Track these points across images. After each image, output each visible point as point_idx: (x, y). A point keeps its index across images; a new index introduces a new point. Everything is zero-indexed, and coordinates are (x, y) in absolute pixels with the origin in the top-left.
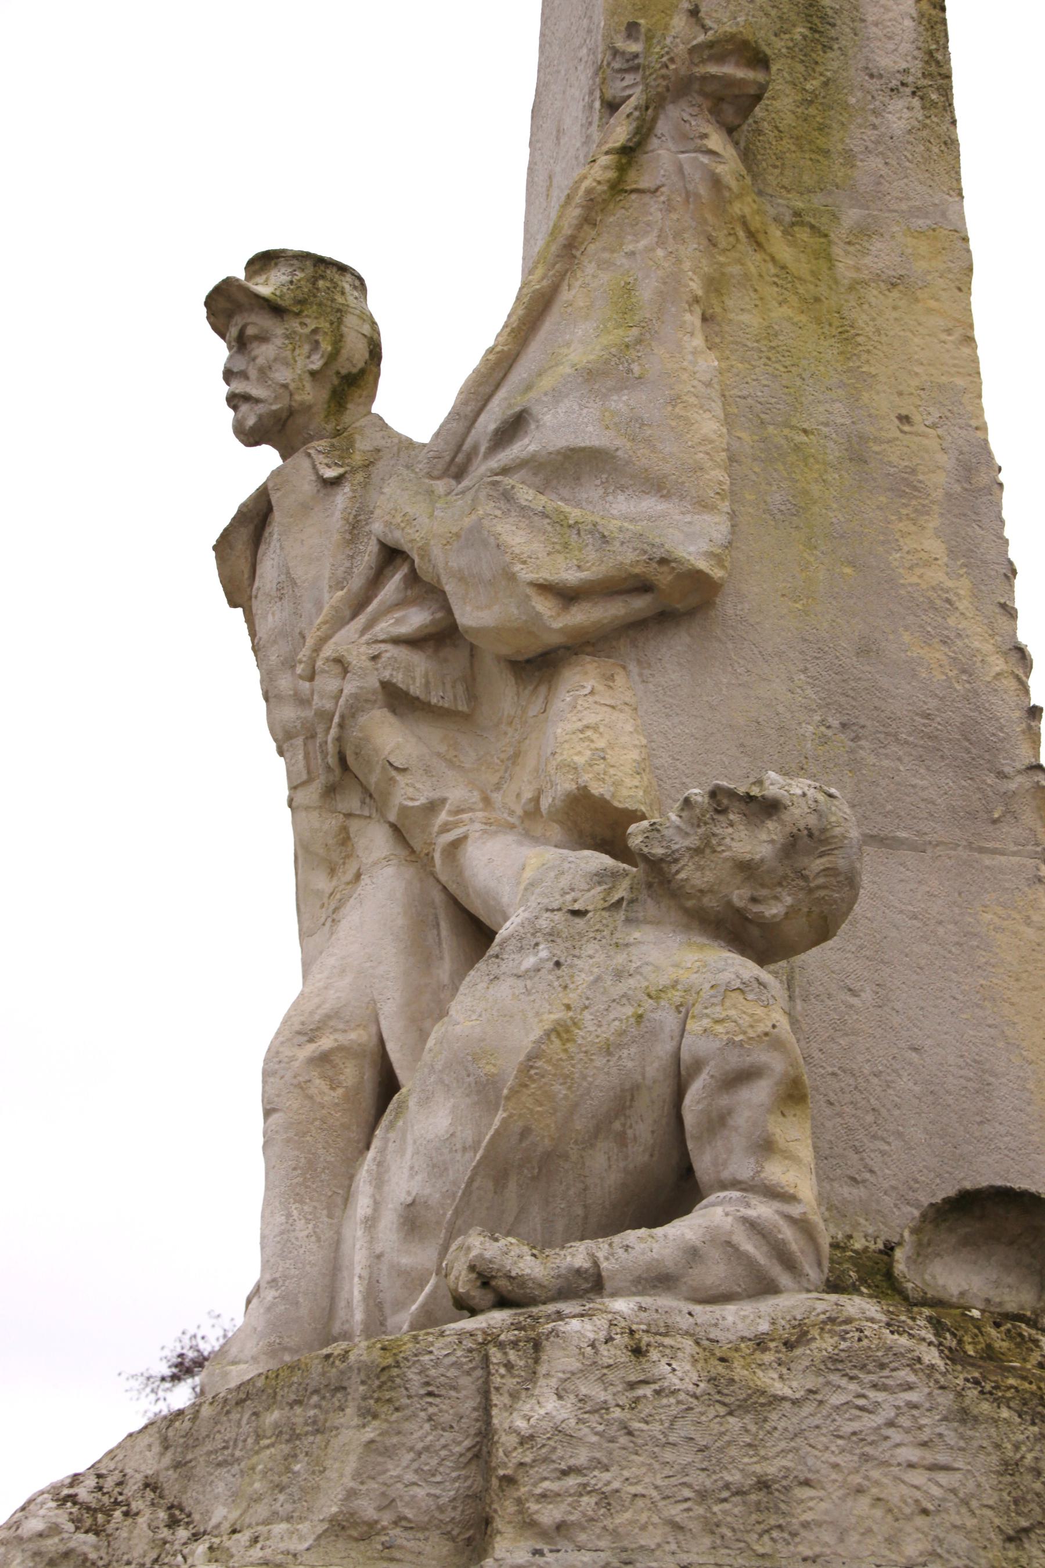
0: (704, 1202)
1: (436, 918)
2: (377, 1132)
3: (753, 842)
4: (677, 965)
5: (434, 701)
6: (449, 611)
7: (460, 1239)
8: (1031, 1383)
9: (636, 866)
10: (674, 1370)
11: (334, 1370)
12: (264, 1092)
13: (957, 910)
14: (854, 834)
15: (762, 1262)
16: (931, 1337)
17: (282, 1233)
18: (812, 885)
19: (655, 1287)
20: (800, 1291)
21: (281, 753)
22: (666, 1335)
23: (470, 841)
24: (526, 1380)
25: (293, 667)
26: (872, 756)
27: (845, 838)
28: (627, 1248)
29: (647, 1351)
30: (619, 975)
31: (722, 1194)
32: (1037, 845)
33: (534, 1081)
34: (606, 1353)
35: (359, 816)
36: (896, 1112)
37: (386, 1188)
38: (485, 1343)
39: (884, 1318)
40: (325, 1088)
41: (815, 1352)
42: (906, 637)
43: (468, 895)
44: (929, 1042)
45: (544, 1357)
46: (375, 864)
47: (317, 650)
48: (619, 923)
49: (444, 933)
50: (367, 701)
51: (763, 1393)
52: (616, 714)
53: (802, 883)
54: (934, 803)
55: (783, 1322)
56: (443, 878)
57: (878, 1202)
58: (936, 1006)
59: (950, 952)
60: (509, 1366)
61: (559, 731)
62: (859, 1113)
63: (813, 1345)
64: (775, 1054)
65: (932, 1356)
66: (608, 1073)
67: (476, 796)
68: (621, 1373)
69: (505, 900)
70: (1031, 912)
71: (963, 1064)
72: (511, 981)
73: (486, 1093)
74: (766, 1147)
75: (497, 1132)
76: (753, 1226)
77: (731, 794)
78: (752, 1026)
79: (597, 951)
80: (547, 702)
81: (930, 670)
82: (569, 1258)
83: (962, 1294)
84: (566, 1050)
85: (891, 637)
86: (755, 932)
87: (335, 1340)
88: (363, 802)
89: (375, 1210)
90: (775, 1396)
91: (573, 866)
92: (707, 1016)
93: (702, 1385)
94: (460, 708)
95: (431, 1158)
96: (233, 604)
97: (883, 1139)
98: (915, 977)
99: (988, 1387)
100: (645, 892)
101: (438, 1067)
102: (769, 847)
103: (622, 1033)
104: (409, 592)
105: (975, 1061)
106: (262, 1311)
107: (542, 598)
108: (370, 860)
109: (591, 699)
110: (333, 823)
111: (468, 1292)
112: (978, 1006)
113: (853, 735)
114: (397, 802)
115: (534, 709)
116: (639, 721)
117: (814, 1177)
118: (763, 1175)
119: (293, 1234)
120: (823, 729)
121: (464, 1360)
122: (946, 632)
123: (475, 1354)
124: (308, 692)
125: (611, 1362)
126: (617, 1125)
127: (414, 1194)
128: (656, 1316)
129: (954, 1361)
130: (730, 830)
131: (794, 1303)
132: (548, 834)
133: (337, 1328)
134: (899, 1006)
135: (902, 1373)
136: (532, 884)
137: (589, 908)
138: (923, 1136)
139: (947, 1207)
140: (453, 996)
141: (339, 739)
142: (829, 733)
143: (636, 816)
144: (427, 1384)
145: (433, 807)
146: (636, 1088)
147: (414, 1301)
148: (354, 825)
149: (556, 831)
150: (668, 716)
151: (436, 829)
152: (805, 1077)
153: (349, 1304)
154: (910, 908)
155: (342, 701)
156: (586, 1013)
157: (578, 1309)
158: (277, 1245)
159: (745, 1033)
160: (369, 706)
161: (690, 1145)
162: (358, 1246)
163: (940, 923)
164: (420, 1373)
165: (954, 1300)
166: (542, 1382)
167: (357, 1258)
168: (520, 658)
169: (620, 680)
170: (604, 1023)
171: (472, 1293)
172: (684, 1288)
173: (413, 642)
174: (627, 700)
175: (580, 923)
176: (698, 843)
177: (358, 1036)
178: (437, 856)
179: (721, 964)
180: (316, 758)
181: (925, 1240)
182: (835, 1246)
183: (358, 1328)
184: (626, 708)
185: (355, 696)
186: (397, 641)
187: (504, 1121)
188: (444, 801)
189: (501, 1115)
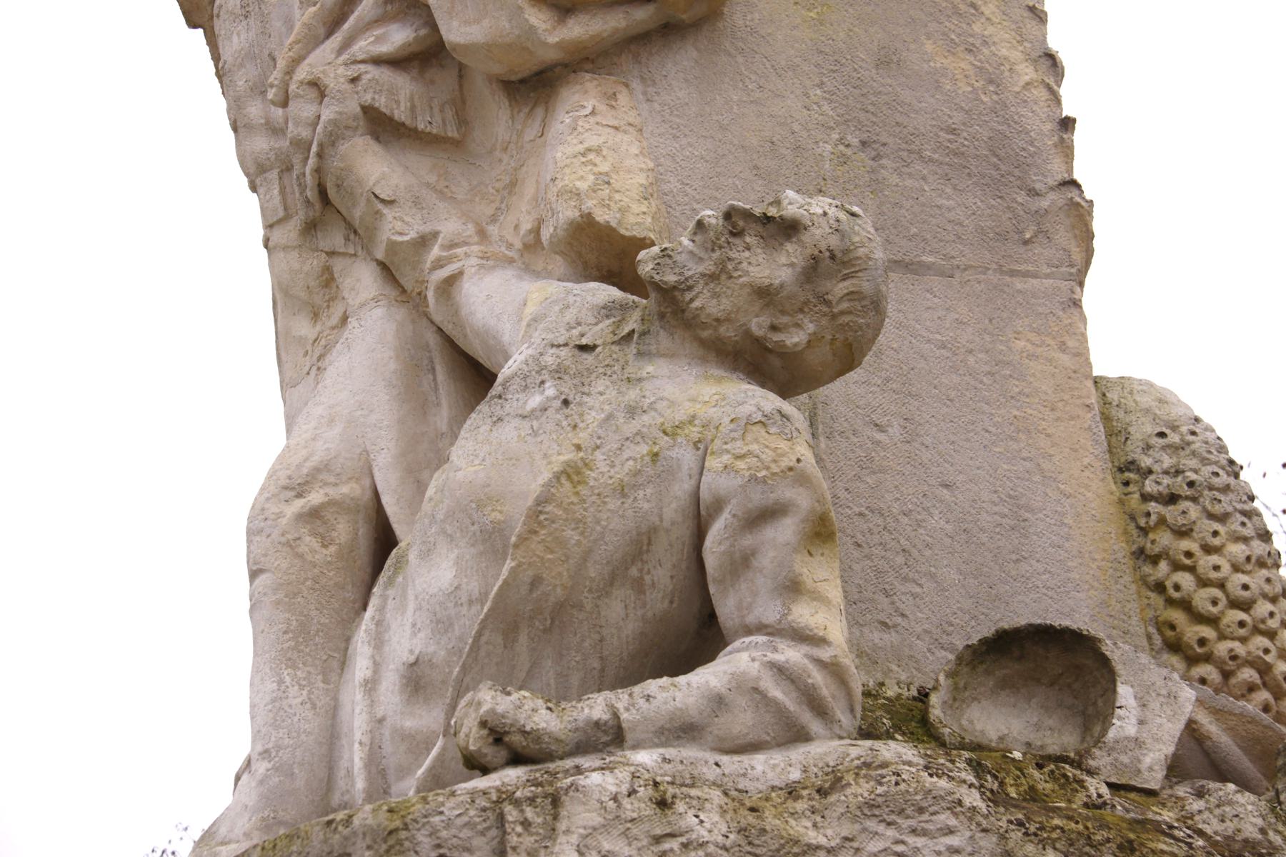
0: (729, 648)
1: (432, 362)
2: (375, 590)
3: (773, 267)
4: (693, 400)
5: (421, 127)
6: (434, 28)
7: (469, 695)
8: (1077, 823)
9: (646, 297)
10: (702, 822)
11: (337, 836)
12: (249, 552)
13: (987, 338)
14: (879, 254)
15: (792, 709)
16: (971, 778)
17: (273, 701)
18: (835, 310)
19: (679, 737)
20: (832, 738)
21: (254, 188)
22: (692, 786)
23: (465, 277)
24: (545, 838)
25: (264, 93)
26: (895, 176)
27: (870, 259)
28: (648, 698)
29: (673, 803)
30: (632, 411)
31: (747, 640)
32: (1072, 266)
33: (544, 527)
34: (629, 807)
35: (344, 254)
36: (928, 553)
37: (386, 649)
38: (499, 802)
39: (922, 762)
40: (316, 546)
41: (851, 798)
42: (929, 47)
43: (465, 336)
44: (961, 478)
45: (564, 813)
46: (362, 305)
47: (289, 72)
48: (631, 357)
49: (441, 377)
50: (347, 127)
51: (797, 842)
52: (620, 135)
53: (825, 309)
54: (961, 224)
55: (815, 770)
56: (437, 318)
57: (911, 647)
58: (968, 440)
59: (981, 382)
60: (526, 824)
61: (559, 155)
62: (888, 554)
63: (848, 791)
64: (801, 489)
65: (973, 798)
66: (623, 516)
67: (471, 229)
68: (646, 826)
69: (506, 339)
70: (1066, 338)
71: (997, 500)
72: (517, 422)
73: (492, 541)
74: (793, 588)
75: (505, 582)
76: (781, 671)
77: (747, 215)
78: (775, 461)
79: (607, 387)
80: (544, 125)
81: (955, 81)
82: (586, 711)
83: (1001, 739)
84: (577, 493)
85: (912, 46)
86: (776, 362)
87: (335, 811)
88: (347, 239)
89: (376, 672)
90: (809, 845)
91: (578, 299)
92: (728, 451)
93: (732, 836)
94: (450, 134)
95: (435, 614)
96: (192, 24)
97: (914, 581)
98: (945, 410)
99: (1032, 829)
100: (657, 323)
101: (440, 516)
102: (789, 271)
103: (637, 473)
104: (389, 7)
105: (1010, 497)
106: (253, 784)
107: (536, 10)
108: (357, 301)
109: (592, 120)
110: (314, 263)
111: (479, 749)
112: (1012, 438)
113: (874, 153)
114: (384, 238)
115: (531, 133)
116: (645, 144)
117: (843, 618)
118: (790, 618)
119: (285, 702)
120: (841, 148)
121: (478, 820)
122: (971, 40)
123: (489, 813)
124: (281, 120)
125: (635, 815)
126: (634, 572)
127: (417, 652)
128: (681, 767)
129: (996, 803)
130: (747, 254)
131: (825, 750)
132: (550, 268)
133: (336, 799)
134: (928, 441)
135: (942, 817)
136: (535, 320)
137: (598, 342)
138: (956, 577)
139: (984, 648)
140: (452, 444)
141: (318, 170)
142: (849, 152)
143: (644, 243)
144: (439, 846)
145: (424, 242)
146: (653, 530)
147: (420, 767)
148: (338, 265)
149: (558, 264)
150: (675, 137)
151: (428, 265)
152: (833, 514)
153: (349, 773)
154: (939, 337)
155: (319, 129)
156: (597, 453)
157: (598, 763)
158: (269, 716)
159: (768, 468)
160: (348, 133)
161: (712, 589)
162: (357, 711)
163: (971, 352)
164: (430, 835)
165: (993, 745)
166: (562, 839)
167: (357, 722)
168: (513, 78)
169: (623, 99)
170: (617, 462)
171: (485, 751)
172: (710, 739)
173: (396, 62)
174: (631, 120)
175: (588, 358)
176: (713, 268)
177: (350, 490)
178: (430, 295)
179: (741, 397)
180: (293, 193)
181: (962, 684)
182: (867, 694)
183: (359, 798)
184: (631, 129)
185: (334, 122)
186: (378, 61)
187: (513, 571)
188: (435, 235)
189: (509, 564)
